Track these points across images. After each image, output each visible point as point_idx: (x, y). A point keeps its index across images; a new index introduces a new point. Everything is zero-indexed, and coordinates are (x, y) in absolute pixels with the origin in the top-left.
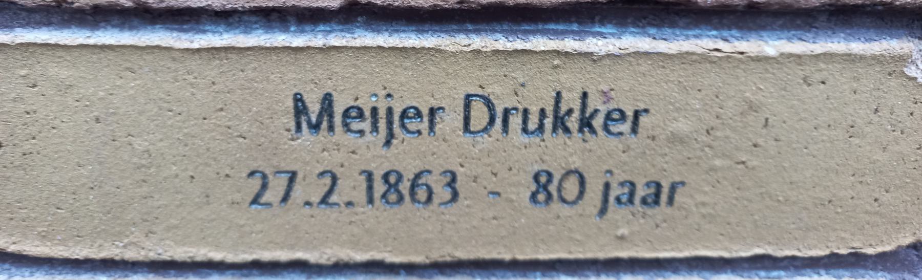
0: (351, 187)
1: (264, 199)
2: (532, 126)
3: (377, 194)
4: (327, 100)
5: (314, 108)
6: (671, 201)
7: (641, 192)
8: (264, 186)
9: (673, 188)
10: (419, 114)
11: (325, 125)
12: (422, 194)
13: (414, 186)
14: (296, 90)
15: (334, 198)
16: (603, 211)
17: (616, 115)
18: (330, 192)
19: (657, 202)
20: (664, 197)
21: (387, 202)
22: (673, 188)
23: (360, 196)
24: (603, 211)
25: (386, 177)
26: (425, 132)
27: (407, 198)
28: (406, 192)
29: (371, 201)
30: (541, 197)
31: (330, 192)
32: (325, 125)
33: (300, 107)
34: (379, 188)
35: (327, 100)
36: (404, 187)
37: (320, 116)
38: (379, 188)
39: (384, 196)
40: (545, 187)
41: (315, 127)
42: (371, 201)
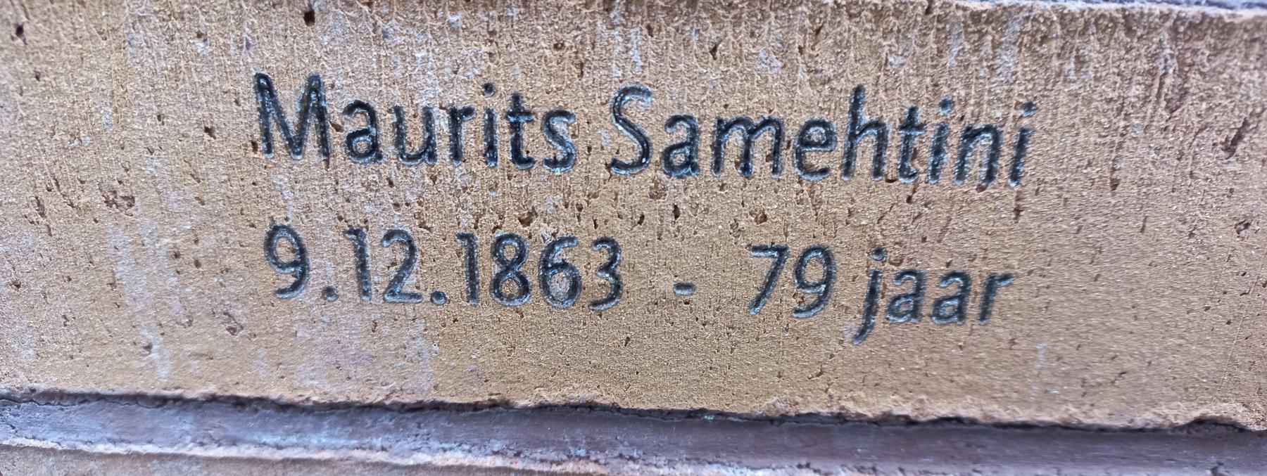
0: (440, 267)
5: (289, 98)
7: (933, 290)
9: (991, 285)
11: (312, 135)
12: (560, 283)
13: (547, 266)
14: (313, 70)
15: (409, 284)
17: (816, 134)
20: (973, 308)
21: (500, 295)
22: (991, 285)
23: (456, 286)
26: (836, 172)
28: (532, 279)
29: (473, 295)
30: (510, 287)
34: (488, 269)
37: (303, 115)
38: (488, 269)
39: (496, 283)
40: (507, 267)
41: (295, 145)
42: (473, 295)
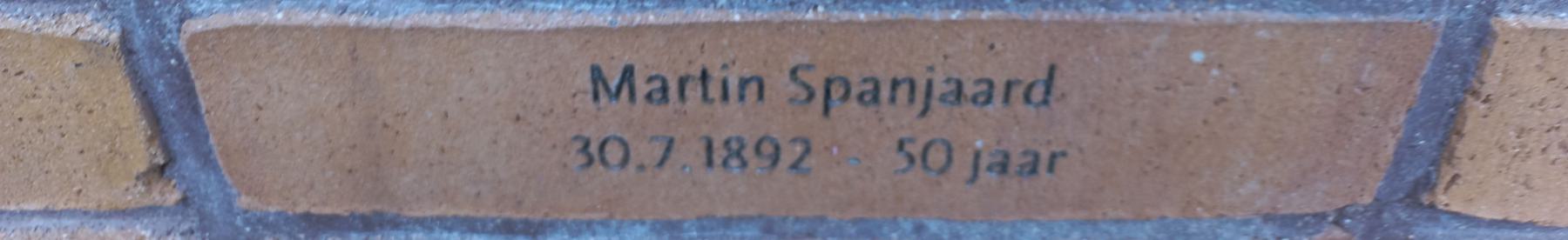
1: (804, 165)
2: (753, 87)
3: (717, 160)
4: (628, 73)
6: (1051, 168)
8: (807, 151)
10: (861, 97)
16: (974, 177)
18: (801, 159)
19: (1034, 171)
20: (1043, 167)
24: (974, 177)
25: (727, 143)
27: (918, 161)
29: (710, 163)
31: (801, 159)
32: (625, 92)
33: (597, 75)
34: (719, 154)
35: (628, 73)
36: (594, 149)
40: (738, 154)
42: (710, 163)
